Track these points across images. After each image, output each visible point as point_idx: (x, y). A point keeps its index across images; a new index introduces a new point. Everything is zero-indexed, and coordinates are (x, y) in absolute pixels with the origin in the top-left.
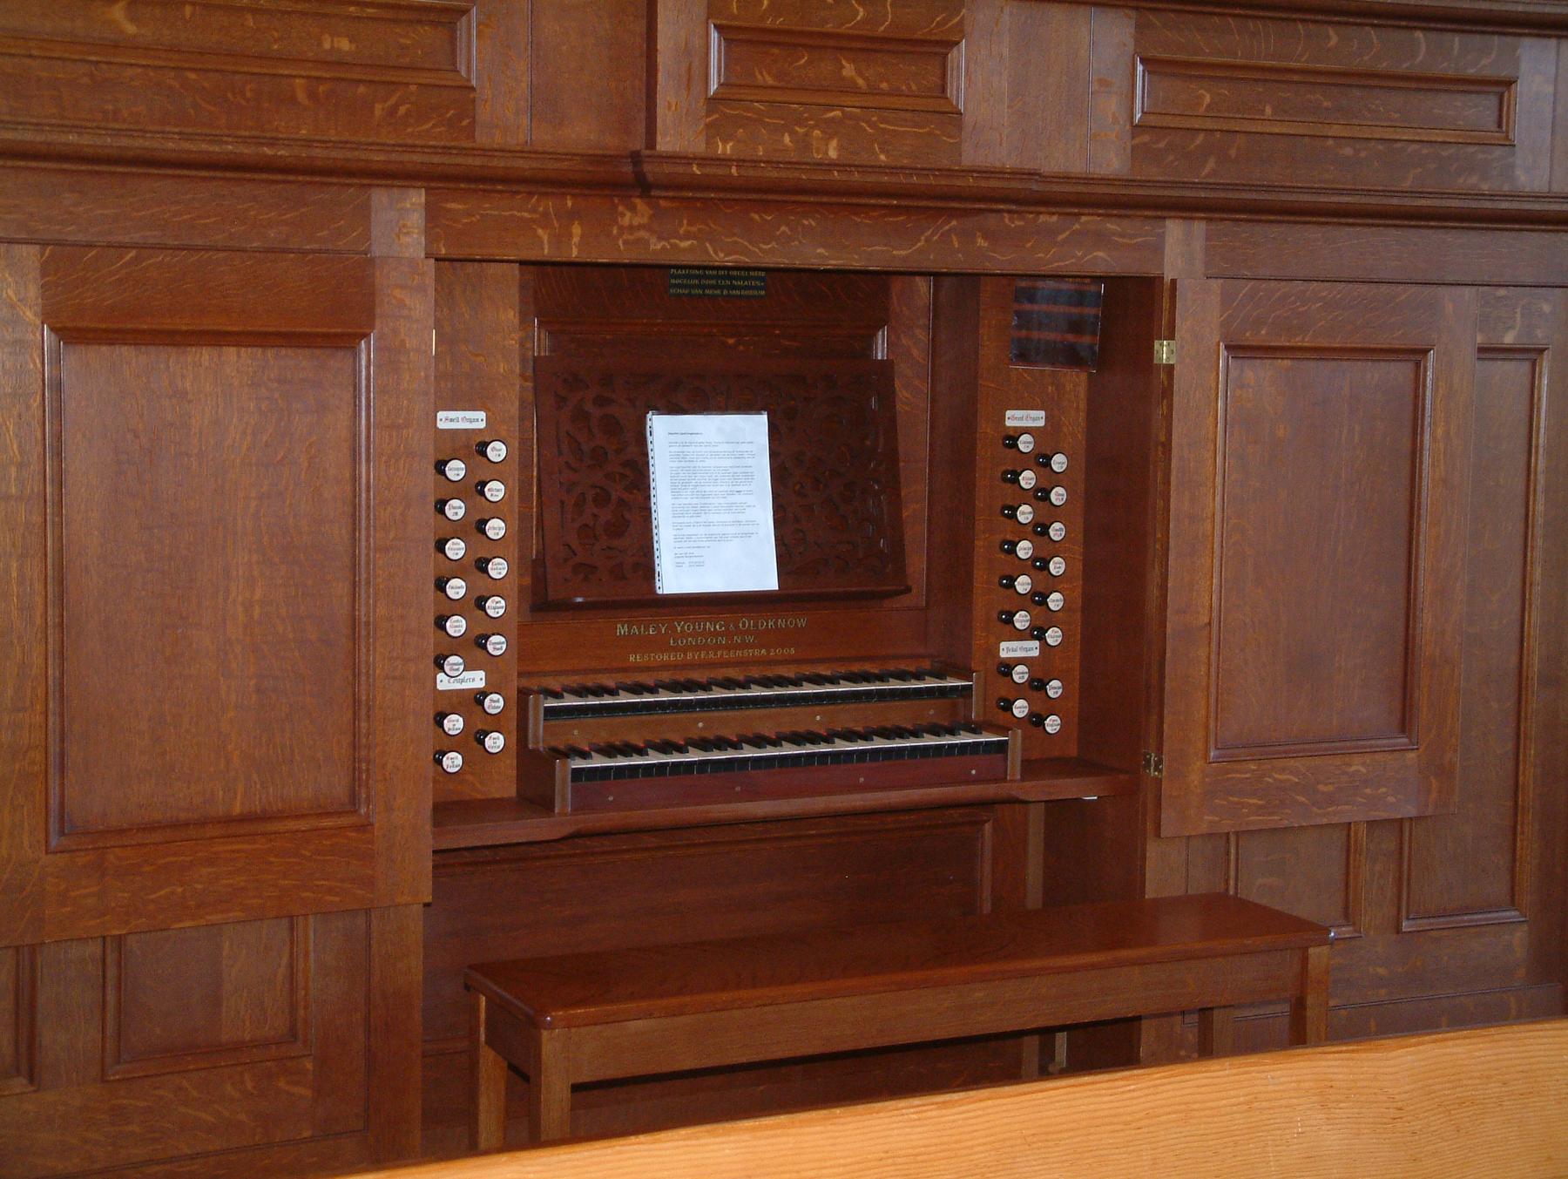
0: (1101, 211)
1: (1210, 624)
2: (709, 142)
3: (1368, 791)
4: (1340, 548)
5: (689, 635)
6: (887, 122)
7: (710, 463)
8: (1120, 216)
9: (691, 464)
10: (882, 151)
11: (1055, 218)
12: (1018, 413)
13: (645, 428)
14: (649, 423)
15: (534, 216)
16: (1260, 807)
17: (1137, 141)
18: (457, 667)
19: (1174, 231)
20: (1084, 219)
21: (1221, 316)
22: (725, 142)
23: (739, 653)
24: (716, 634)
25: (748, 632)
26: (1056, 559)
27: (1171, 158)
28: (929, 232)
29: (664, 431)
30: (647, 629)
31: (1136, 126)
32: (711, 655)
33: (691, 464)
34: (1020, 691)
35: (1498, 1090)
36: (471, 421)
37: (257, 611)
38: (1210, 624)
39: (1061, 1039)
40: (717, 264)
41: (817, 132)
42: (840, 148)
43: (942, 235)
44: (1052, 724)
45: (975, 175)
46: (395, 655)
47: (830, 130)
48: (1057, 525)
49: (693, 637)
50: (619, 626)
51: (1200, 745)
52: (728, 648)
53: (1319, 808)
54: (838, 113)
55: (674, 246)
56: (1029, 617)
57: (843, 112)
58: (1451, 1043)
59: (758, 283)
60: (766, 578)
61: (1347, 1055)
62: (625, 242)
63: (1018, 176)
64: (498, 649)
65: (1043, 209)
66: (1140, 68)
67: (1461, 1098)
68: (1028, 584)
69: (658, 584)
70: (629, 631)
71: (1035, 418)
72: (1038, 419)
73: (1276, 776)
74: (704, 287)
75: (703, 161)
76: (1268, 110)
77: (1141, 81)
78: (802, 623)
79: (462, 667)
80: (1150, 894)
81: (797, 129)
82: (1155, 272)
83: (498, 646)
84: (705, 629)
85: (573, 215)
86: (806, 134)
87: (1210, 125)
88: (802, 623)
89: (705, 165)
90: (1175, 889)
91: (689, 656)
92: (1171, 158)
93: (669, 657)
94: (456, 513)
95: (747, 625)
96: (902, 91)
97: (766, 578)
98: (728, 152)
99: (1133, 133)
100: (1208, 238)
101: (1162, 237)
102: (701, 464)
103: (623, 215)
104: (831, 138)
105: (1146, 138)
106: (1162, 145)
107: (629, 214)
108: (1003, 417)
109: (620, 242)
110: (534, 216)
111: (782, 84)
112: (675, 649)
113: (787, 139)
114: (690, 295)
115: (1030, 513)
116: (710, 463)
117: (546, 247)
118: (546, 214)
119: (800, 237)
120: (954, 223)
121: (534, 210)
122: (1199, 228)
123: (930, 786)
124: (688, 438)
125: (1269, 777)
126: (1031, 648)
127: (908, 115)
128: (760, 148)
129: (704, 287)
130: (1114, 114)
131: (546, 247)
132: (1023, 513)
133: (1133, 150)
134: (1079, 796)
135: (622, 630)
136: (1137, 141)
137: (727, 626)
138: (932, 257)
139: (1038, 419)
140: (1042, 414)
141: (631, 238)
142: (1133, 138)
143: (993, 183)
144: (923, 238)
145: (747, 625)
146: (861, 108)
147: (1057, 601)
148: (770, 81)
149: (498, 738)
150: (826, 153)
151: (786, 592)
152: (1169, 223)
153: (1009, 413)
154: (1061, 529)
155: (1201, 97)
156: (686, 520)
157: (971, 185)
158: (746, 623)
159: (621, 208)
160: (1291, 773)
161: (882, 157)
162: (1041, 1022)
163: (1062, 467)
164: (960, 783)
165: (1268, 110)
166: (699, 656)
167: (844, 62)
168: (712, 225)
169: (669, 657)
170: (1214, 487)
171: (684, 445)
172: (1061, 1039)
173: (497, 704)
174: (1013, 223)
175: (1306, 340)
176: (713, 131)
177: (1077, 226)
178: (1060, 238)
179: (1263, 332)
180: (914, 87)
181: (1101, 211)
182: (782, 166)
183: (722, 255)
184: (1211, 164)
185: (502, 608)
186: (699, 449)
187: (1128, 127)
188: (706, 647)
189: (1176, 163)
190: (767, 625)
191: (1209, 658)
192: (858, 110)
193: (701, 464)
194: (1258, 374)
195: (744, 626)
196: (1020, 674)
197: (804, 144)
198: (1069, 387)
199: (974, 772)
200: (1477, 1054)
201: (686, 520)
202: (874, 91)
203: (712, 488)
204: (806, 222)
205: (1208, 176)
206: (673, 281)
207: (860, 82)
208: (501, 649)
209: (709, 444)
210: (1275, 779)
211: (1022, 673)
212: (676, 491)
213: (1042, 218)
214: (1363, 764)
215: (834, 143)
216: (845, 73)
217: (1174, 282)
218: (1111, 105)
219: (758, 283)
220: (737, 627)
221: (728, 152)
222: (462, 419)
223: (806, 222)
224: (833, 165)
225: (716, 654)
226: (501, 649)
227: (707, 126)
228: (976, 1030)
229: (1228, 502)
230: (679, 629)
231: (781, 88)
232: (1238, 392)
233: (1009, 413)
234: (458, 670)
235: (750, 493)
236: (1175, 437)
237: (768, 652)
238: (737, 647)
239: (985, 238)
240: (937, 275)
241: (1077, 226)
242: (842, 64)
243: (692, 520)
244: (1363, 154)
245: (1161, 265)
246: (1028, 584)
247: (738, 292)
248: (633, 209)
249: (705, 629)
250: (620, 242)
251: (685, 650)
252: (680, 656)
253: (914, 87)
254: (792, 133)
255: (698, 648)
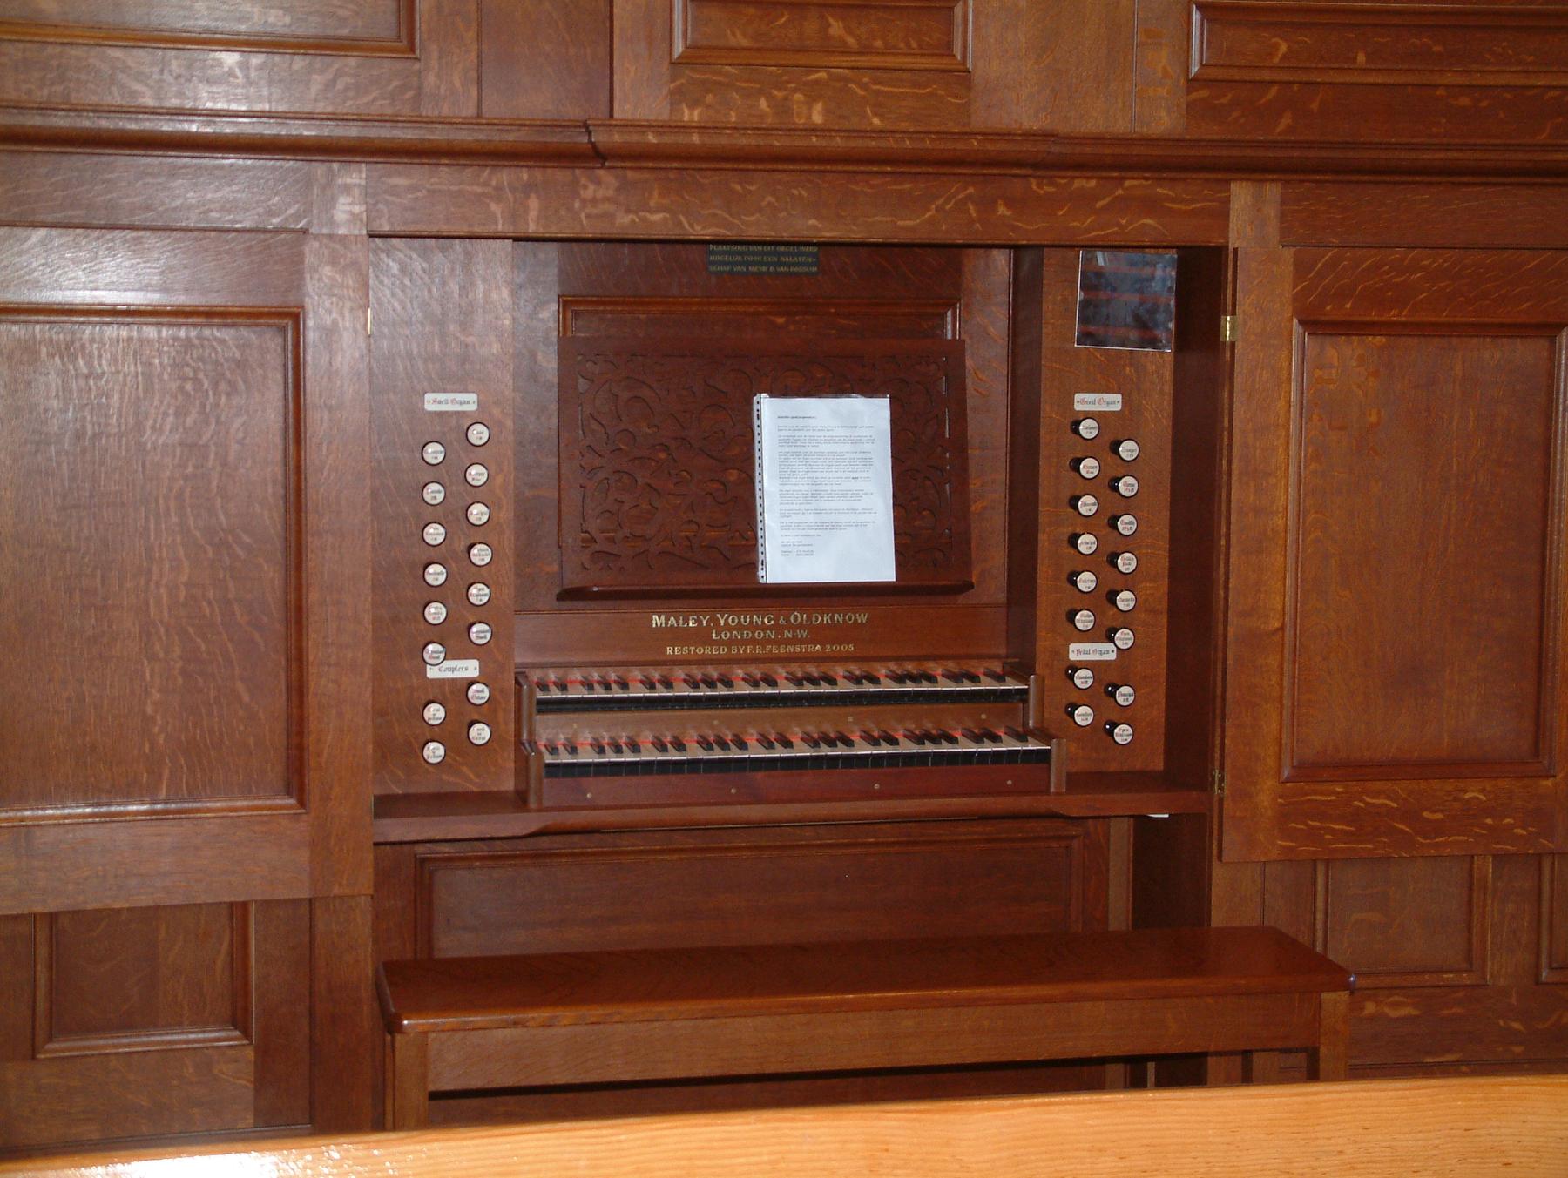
0: (1147, 175)
1: (1282, 628)
2: (674, 107)
3: (1489, 821)
4: (1451, 547)
5: (734, 628)
6: (880, 83)
7: (825, 448)
8: (1172, 180)
9: (802, 449)
10: (875, 114)
11: (1093, 183)
12: (441, 396)
13: (752, 409)
14: (756, 407)
15: (487, 190)
16: (1352, 833)
17: (1194, 96)
18: (436, 655)
19: (1241, 195)
20: (1127, 183)
21: (1294, 289)
22: (692, 107)
23: (791, 648)
24: (764, 628)
25: (801, 626)
26: (1126, 555)
27: (1235, 114)
28: (942, 200)
29: (771, 412)
30: (686, 620)
31: (1194, 80)
32: (758, 650)
33: (802, 449)
34: (1087, 697)
35: (1113, 1164)
36: (1108, 403)
37: (183, 593)
38: (1282, 628)
39: (1151, 1067)
40: (692, 237)
41: (798, 96)
42: (827, 112)
43: (956, 204)
44: (1123, 734)
45: (980, 138)
46: (330, 641)
47: (814, 93)
48: (1127, 518)
49: (738, 630)
50: (655, 617)
51: (1271, 762)
52: (777, 642)
53: (1425, 837)
54: (822, 75)
55: (644, 220)
56: (1092, 617)
57: (828, 73)
58: (1057, 1108)
59: (810, 260)
60: (880, 567)
61: (914, 1116)
62: (588, 216)
63: (1031, 138)
64: (482, 638)
65: (1077, 174)
66: (1196, 16)
67: (1061, 1171)
68: (1092, 581)
69: (761, 573)
70: (666, 624)
71: (1112, 402)
72: (1113, 402)
73: (1368, 800)
74: (748, 264)
75: (659, 128)
76: (1361, 58)
77: (1198, 29)
78: (862, 618)
79: (442, 656)
80: (1218, 919)
81: (775, 92)
82: (1217, 241)
83: (482, 635)
84: (751, 622)
85: (529, 188)
86: (786, 99)
87: (1286, 77)
88: (862, 618)
89: (662, 134)
90: (1249, 917)
91: (734, 651)
92: (1235, 114)
93: (711, 651)
94: (435, 498)
95: (799, 619)
96: (900, 49)
97: (880, 567)
98: (696, 119)
99: (1188, 88)
100: (1283, 202)
101: (1227, 201)
102: (813, 449)
103: (585, 187)
104: (815, 100)
105: (1204, 93)
106: (1224, 100)
107: (591, 188)
108: (1124, 403)
109: (583, 216)
110: (487, 190)
111: (760, 45)
112: (719, 643)
113: (763, 104)
114: (731, 273)
115: (1094, 504)
116: (825, 448)
117: (500, 222)
118: (498, 188)
119: (789, 207)
120: (971, 190)
121: (486, 184)
122: (1273, 191)
123: (952, 795)
124: (801, 422)
125: (1360, 801)
126: (1104, 652)
127: (906, 75)
128: (733, 114)
129: (748, 264)
130: (1164, 68)
131: (500, 222)
132: (1085, 504)
133: (1188, 106)
134: (1144, 813)
135: (657, 621)
136: (1194, 96)
137: (777, 620)
138: (944, 228)
139: (1113, 402)
140: (1118, 397)
141: (595, 211)
142: (1189, 93)
143: (1001, 146)
144: (933, 207)
145: (799, 619)
146: (853, 68)
147: (1128, 600)
148: (745, 43)
149: (483, 730)
150: (809, 117)
151: (903, 583)
152: (1234, 187)
153: (1078, 397)
154: (1131, 523)
155: (1276, 46)
156: (795, 507)
157: (976, 148)
158: (798, 617)
159: (583, 181)
160: (1388, 797)
161: (876, 121)
162: (1126, 1049)
163: (1132, 455)
164: (989, 794)
165: (1361, 58)
166: (745, 651)
167: (831, 21)
168: (687, 197)
169: (711, 651)
170: (1287, 478)
171: (796, 428)
172: (1151, 1067)
173: (481, 695)
174: (1042, 189)
175: (1404, 313)
176: (678, 97)
177: (1120, 192)
178: (1099, 204)
179: (1348, 306)
180: (914, 45)
181: (1147, 175)
182: (749, 132)
183: (698, 228)
184: (1286, 121)
185: (485, 595)
186: (811, 433)
187: (1182, 81)
188: (753, 642)
189: (1242, 120)
190: (823, 620)
191: (1281, 667)
192: (847, 71)
193: (813, 449)
194: (1344, 354)
195: (796, 620)
196: (1083, 678)
197: (783, 108)
198: (1151, 368)
199: (1009, 782)
200: (1090, 1122)
201: (795, 507)
202: (865, 50)
203: (825, 475)
204: (795, 192)
205: (1279, 134)
206: (712, 258)
207: (851, 40)
208: (485, 637)
209: (822, 428)
210: (1367, 804)
211: (1086, 678)
212: (784, 478)
213: (1077, 183)
214: (1483, 791)
215: (818, 107)
216: (831, 31)
217: (1235, 250)
218: (1162, 59)
219: (810, 260)
220: (788, 620)
221: (696, 119)
222: (452, 401)
223: (795, 192)
224: (814, 130)
225: (764, 649)
226: (485, 637)
227: (671, 93)
228: (905, 1061)
229: (1305, 495)
230: (722, 622)
231: (759, 50)
232: (1318, 373)
233: (1078, 397)
234: (438, 658)
235: (867, 479)
236: (1236, 423)
237: (823, 648)
238: (787, 642)
239: (1008, 205)
240: (1016, 248)
241: (1120, 192)
242: (827, 21)
243: (803, 507)
244: (1484, 104)
245: (1226, 238)
246: (1092, 581)
247: (786, 269)
248: (598, 182)
249: (751, 622)
250: (583, 216)
251: (730, 643)
252: (724, 650)
253: (914, 45)
254: (770, 98)
255: (743, 642)
